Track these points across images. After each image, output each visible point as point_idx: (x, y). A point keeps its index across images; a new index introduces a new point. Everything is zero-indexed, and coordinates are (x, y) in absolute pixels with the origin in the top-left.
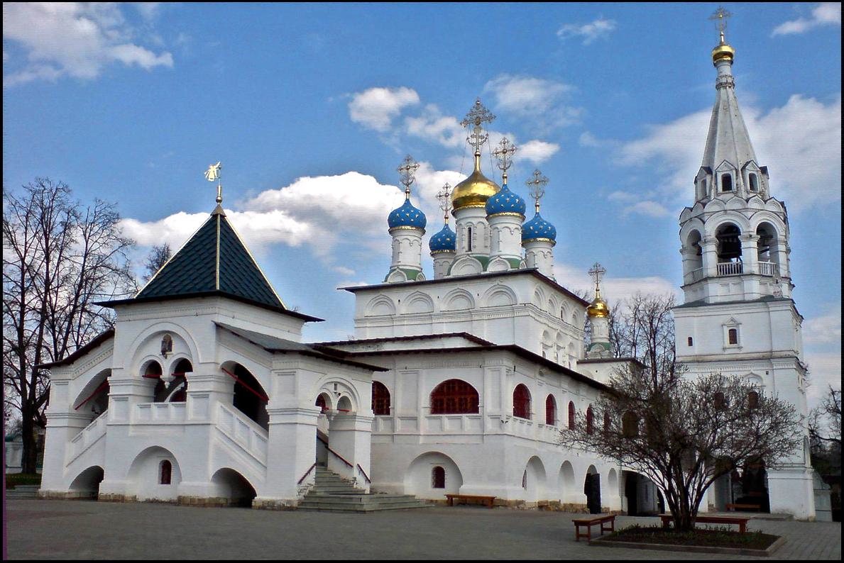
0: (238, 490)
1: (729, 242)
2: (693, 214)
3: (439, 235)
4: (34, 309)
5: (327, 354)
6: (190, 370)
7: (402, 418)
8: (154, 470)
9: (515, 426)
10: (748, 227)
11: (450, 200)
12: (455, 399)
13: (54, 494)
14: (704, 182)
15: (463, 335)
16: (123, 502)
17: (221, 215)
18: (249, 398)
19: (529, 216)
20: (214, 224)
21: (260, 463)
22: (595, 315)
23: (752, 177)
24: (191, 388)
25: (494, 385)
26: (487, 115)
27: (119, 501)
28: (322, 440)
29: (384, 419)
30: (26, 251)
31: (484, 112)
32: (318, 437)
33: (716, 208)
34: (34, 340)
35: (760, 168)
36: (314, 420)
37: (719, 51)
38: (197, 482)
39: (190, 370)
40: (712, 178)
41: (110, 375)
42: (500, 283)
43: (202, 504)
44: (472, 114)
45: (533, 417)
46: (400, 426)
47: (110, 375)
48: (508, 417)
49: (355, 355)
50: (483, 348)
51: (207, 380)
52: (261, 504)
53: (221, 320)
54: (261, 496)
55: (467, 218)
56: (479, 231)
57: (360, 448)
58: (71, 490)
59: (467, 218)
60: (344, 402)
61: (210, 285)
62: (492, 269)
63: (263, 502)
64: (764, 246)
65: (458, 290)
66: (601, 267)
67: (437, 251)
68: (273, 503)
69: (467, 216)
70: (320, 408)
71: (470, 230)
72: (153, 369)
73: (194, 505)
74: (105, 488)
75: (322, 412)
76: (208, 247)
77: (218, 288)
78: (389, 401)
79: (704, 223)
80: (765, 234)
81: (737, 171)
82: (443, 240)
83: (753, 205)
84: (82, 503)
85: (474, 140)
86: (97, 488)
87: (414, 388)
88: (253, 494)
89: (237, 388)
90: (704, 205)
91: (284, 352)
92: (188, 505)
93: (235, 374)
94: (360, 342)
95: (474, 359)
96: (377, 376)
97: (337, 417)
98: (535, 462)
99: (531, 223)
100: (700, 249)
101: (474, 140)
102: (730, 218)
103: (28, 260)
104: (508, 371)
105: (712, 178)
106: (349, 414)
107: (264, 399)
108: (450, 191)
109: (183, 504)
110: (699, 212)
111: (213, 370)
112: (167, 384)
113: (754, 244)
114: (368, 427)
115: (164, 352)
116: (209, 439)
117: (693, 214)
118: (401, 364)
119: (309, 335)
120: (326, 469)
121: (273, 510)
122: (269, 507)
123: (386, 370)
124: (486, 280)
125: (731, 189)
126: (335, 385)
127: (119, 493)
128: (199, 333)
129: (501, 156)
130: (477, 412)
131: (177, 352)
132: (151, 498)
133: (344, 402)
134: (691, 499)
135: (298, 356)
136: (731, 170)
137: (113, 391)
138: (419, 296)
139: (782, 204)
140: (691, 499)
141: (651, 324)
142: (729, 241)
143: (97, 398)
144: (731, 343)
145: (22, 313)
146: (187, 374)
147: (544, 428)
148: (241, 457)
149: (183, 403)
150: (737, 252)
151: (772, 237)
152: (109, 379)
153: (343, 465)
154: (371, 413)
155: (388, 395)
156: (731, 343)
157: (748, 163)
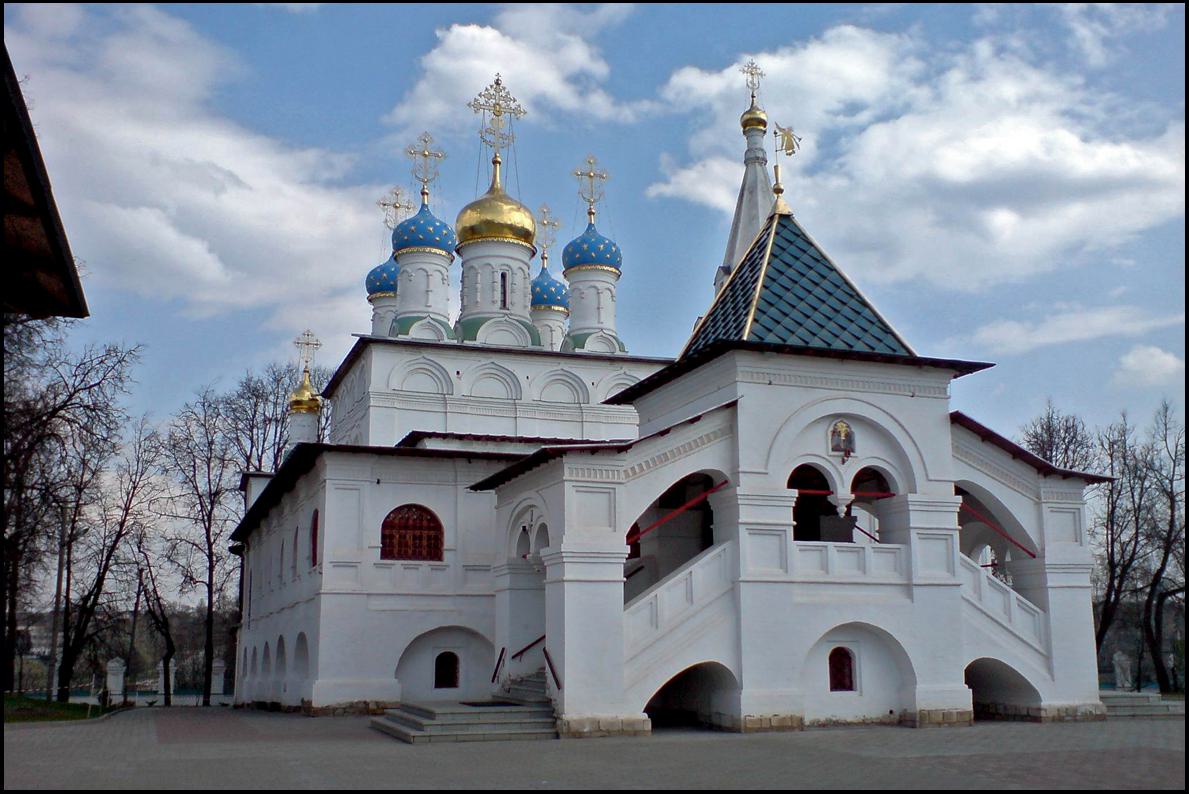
0: (994, 692)
7: (337, 565)
13: (612, 724)
16: (802, 730)
21: (1031, 647)
27: (791, 728)
37: (752, 116)
42: (628, 373)
43: (946, 720)
51: (930, 509)
52: (1056, 713)
55: (504, 257)
59: (489, 256)
62: (416, 333)
63: (1058, 710)
65: (562, 372)
66: (315, 338)
67: (379, 294)
68: (1075, 709)
69: (491, 253)
71: (503, 276)
73: (951, 724)
92: (939, 724)
109: (930, 723)
121: (1076, 720)
124: (607, 364)
127: (789, 714)
128: (777, 422)
129: (420, 159)
132: (822, 719)
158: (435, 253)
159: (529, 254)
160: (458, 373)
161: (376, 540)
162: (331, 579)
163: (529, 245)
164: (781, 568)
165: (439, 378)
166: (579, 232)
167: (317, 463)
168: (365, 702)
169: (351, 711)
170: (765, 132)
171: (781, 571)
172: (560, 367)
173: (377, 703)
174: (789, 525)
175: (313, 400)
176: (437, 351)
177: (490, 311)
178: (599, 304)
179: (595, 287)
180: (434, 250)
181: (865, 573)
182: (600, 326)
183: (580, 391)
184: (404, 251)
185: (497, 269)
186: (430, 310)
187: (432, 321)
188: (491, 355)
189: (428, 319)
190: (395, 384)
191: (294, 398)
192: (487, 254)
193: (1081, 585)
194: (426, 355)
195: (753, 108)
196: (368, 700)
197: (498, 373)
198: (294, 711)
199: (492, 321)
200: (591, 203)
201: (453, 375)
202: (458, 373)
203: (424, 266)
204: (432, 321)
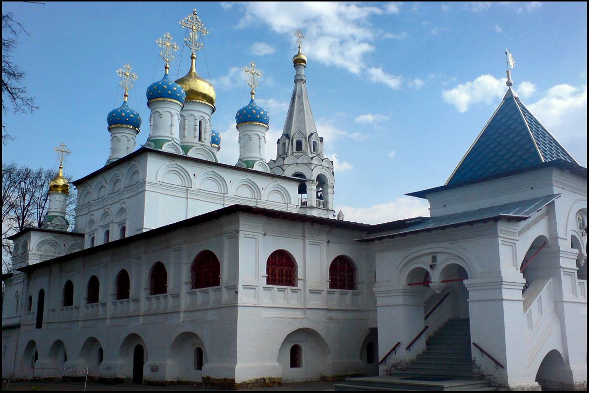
2: (276, 164)
14: (284, 144)
23: (314, 143)
33: (291, 161)
35: (320, 138)
37: (299, 57)
40: (289, 141)
42: (280, 184)
55: (189, 110)
59: (189, 110)
65: (247, 180)
71: (200, 123)
79: (284, 171)
80: (321, 181)
81: (305, 139)
83: (314, 161)
90: (284, 159)
102: (301, 169)
105: (289, 141)
110: (280, 163)
117: (276, 164)
125: (301, 150)
136: (302, 138)
138: (212, 176)
139: (332, 162)
144: (330, 288)
148: (566, 181)
149: (128, 299)
151: (325, 183)
156: (330, 288)
157: (312, 134)
158: (174, 103)
159: (211, 111)
160: (194, 175)
161: (263, 272)
162: (244, 298)
163: (212, 106)
164: (573, 294)
165: (182, 176)
166: (245, 103)
167: (224, 216)
168: (264, 379)
169: (257, 385)
170: (305, 67)
171: (573, 296)
172: (247, 178)
173: (270, 379)
174: (575, 270)
175: (66, 186)
176: (184, 161)
177: (193, 142)
178: (260, 145)
179: (258, 135)
180: (173, 101)
181: (576, 296)
182: (260, 157)
183: (255, 192)
184: (153, 100)
185: (197, 118)
186: (173, 136)
187: (175, 144)
188: (212, 167)
189: (172, 142)
190: (160, 178)
191: (53, 183)
192: (192, 109)
193: (433, 307)
194: (178, 164)
195: (299, 54)
196: (265, 377)
197: (215, 177)
198: (169, 385)
199: (196, 147)
200: (253, 88)
201: (192, 176)
202: (194, 175)
203: (170, 110)
204: (175, 144)
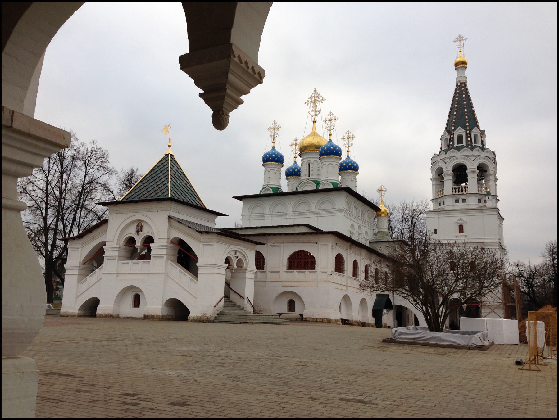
0: (178, 311)
1: (460, 175)
3: (291, 168)
4: (54, 206)
5: (229, 234)
6: (153, 242)
8: (129, 300)
9: (336, 277)
10: (472, 167)
11: (298, 147)
12: (302, 261)
15: (307, 226)
17: (171, 155)
18: (186, 258)
19: (344, 157)
20: (167, 159)
22: (380, 215)
24: (153, 252)
25: (324, 254)
26: (321, 98)
28: (227, 284)
29: (261, 272)
30: (49, 172)
31: (319, 97)
32: (225, 282)
34: (53, 227)
36: (224, 272)
38: (154, 305)
39: (153, 242)
41: (105, 245)
44: (312, 97)
45: (346, 272)
46: (270, 276)
47: (105, 245)
48: (332, 272)
49: (241, 235)
50: (317, 232)
53: (172, 214)
54: (193, 314)
56: (313, 167)
57: (249, 290)
58: (80, 312)
60: (240, 262)
61: (165, 194)
64: (481, 176)
70: (227, 265)
72: (131, 241)
74: (100, 310)
75: (228, 268)
76: (164, 172)
77: (170, 196)
78: (264, 262)
82: (293, 170)
84: (82, 318)
85: (313, 113)
86: (95, 310)
87: (278, 255)
88: (188, 312)
89: (180, 252)
91: (207, 233)
93: (179, 244)
94: (251, 228)
95: (311, 238)
96: (259, 248)
97: (236, 270)
98: (346, 298)
99: (344, 162)
100: (443, 178)
101: (313, 113)
103: (50, 178)
104: (332, 246)
106: (242, 268)
107: (196, 259)
108: (298, 142)
111: (165, 243)
112: (139, 250)
113: (450, 178)
114: (252, 276)
115: (138, 232)
116: (160, 282)
118: (271, 240)
119: (220, 223)
120: (229, 300)
122: (199, 320)
123: (263, 244)
126: (236, 252)
129: (328, 123)
130: (314, 269)
131: (146, 232)
133: (240, 262)
134: (441, 318)
135: (215, 237)
137: (106, 254)
140: (441, 318)
141: (412, 221)
142: (460, 173)
143: (96, 258)
145: (47, 209)
146: (151, 245)
147: (352, 279)
150: (465, 180)
151: (486, 171)
152: (104, 247)
153: (239, 297)
154: (254, 268)
155: (264, 259)
